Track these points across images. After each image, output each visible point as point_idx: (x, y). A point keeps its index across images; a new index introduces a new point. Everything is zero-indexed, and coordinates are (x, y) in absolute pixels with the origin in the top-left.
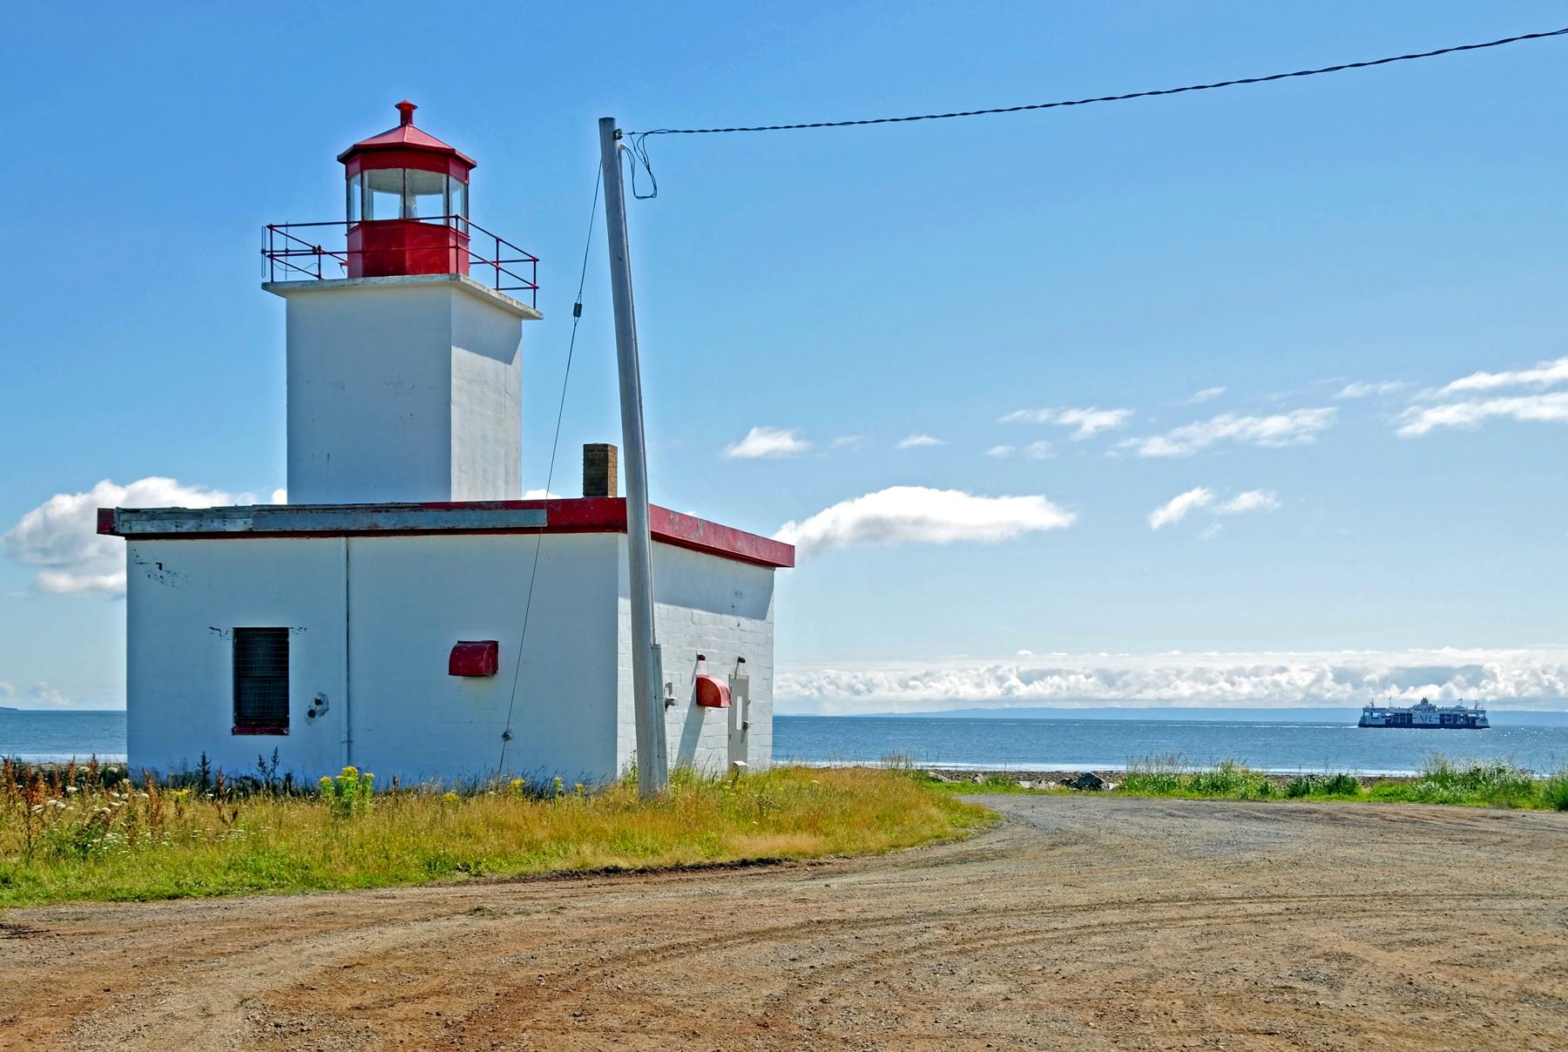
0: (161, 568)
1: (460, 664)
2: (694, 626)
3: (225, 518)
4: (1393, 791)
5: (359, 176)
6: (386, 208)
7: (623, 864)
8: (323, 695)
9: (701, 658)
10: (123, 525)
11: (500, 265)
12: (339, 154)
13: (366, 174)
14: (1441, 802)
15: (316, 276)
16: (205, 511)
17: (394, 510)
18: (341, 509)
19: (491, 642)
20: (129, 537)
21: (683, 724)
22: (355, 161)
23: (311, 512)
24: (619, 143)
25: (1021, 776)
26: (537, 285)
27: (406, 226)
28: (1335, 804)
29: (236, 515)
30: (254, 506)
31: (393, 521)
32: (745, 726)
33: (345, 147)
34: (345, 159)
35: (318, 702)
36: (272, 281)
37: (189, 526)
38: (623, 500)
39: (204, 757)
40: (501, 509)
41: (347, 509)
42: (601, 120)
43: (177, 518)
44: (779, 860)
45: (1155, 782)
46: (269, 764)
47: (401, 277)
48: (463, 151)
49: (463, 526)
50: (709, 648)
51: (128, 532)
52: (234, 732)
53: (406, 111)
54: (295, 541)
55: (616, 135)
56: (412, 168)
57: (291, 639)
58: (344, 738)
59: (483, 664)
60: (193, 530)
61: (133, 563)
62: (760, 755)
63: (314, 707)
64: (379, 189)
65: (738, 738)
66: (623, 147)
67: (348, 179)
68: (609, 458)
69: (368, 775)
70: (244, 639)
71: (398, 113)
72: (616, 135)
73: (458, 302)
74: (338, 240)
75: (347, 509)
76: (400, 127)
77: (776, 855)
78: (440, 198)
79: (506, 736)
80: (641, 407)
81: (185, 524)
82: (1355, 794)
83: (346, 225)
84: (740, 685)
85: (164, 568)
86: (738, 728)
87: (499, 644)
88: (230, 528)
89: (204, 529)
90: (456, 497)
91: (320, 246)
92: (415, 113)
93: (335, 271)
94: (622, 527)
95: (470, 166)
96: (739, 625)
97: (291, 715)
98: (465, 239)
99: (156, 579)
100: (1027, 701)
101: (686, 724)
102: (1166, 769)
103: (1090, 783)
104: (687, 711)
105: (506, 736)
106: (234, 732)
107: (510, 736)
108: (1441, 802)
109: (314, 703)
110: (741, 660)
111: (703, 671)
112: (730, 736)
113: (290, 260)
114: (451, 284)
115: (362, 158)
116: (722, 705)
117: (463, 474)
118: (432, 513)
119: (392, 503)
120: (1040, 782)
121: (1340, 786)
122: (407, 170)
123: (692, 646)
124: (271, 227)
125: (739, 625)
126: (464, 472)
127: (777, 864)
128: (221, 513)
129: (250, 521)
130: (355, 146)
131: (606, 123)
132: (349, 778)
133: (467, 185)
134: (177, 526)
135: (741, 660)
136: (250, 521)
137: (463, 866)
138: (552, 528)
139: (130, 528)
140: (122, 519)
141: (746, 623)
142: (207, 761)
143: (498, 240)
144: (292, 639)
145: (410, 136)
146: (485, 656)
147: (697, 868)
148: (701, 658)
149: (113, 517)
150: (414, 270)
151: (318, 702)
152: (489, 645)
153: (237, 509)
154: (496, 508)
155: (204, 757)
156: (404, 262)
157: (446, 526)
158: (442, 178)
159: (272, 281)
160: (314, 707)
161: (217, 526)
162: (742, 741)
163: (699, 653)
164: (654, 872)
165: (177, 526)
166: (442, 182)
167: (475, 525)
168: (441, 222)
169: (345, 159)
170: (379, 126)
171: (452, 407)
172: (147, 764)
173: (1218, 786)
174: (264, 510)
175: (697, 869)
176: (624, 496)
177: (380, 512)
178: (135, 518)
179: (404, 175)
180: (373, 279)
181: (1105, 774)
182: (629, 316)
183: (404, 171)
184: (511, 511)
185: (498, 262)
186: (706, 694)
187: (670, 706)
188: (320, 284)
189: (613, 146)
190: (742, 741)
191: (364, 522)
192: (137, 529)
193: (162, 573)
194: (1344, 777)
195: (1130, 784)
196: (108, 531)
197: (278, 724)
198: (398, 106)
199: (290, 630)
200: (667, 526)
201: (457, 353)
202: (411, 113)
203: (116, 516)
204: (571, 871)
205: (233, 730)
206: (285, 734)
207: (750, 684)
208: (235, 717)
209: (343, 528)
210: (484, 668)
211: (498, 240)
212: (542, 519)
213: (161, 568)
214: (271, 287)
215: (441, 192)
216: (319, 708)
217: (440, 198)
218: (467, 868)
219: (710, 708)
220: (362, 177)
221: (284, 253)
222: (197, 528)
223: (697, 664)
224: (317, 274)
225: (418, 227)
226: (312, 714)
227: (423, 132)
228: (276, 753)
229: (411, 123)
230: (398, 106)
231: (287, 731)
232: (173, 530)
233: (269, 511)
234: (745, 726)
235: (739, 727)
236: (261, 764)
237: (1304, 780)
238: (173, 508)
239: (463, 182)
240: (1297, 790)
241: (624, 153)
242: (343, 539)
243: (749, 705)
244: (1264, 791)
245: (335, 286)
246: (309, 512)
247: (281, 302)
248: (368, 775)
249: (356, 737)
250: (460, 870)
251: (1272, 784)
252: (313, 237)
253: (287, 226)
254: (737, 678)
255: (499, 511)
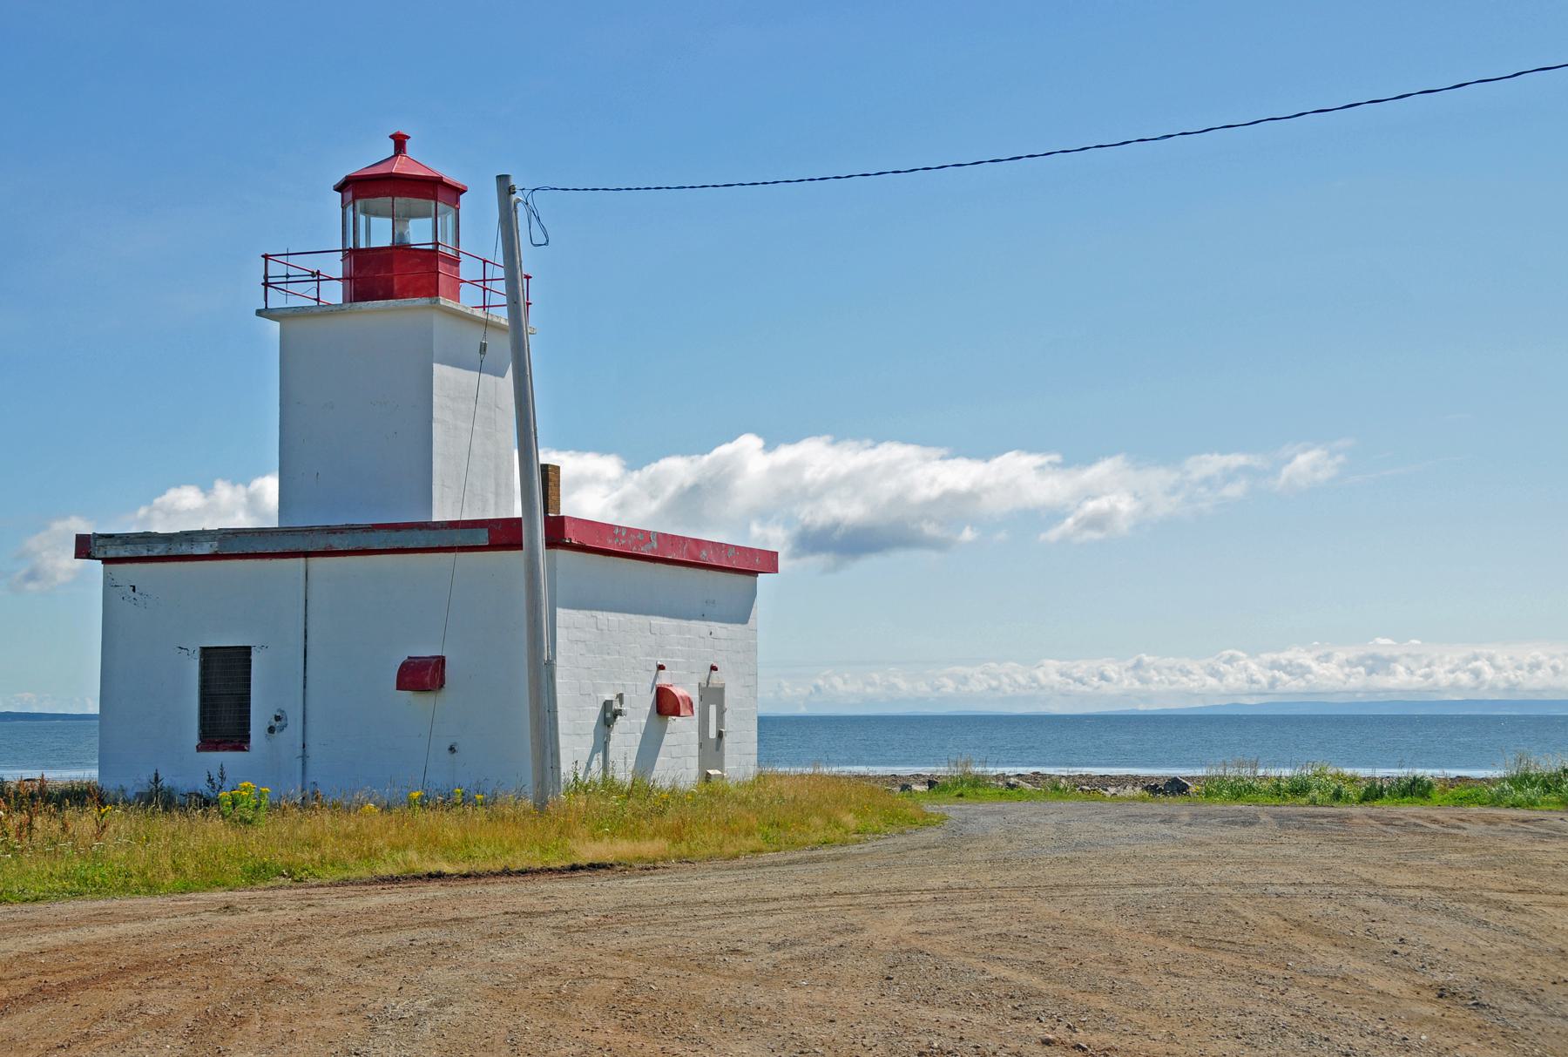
0: (134, 590)
1: (407, 679)
2: (653, 636)
3: (192, 541)
4: (1465, 792)
5: (352, 205)
6: (380, 234)
7: (447, 868)
8: (280, 710)
9: (661, 667)
10: (99, 550)
11: (488, 284)
12: (335, 184)
13: (359, 203)
14: (1512, 805)
15: (315, 299)
16: (174, 535)
17: (348, 531)
18: (298, 531)
19: (439, 657)
20: (106, 561)
21: (640, 736)
22: (348, 190)
23: (272, 535)
24: (514, 197)
25: (1105, 781)
26: (530, 301)
27: (400, 250)
28: (1409, 810)
29: (202, 538)
30: (220, 529)
31: (347, 542)
32: (720, 735)
33: (339, 178)
34: (340, 188)
35: (278, 718)
36: (266, 307)
37: (159, 550)
38: (519, 520)
39: (156, 774)
40: (446, 528)
41: (305, 531)
42: (498, 177)
43: (149, 543)
44: (611, 865)
45: (1231, 788)
46: (217, 780)
47: (385, 301)
48: (451, 175)
49: (411, 546)
50: (672, 658)
51: (103, 556)
52: (199, 749)
53: (400, 142)
54: (258, 562)
55: (511, 191)
56: (400, 196)
57: (253, 657)
58: (299, 752)
59: (428, 679)
60: (163, 554)
61: (109, 585)
62: (740, 762)
63: (274, 723)
64: (376, 215)
65: (713, 748)
66: (519, 200)
67: (344, 208)
68: (550, 477)
69: (264, 789)
70: (209, 656)
71: (392, 142)
72: (511, 191)
73: (439, 322)
74: (334, 266)
75: (305, 531)
76: (393, 157)
77: (610, 859)
78: (429, 221)
79: (452, 749)
80: (536, 438)
81: (157, 548)
82: (1429, 797)
83: (341, 253)
84: (713, 695)
85: (137, 590)
86: (711, 737)
87: (446, 659)
88: (197, 551)
89: (173, 553)
90: (438, 516)
91: (318, 271)
92: (408, 143)
93: (334, 293)
94: (518, 546)
95: (458, 191)
96: (711, 633)
97: (252, 732)
98: (455, 262)
99: (130, 601)
100: (1306, 694)
101: (644, 734)
102: (1246, 772)
103: (1177, 787)
104: (644, 721)
105: (452, 749)
106: (199, 749)
107: (456, 749)
108: (1512, 805)
109: (273, 720)
110: (713, 668)
111: (664, 680)
112: (701, 746)
113: (291, 287)
114: (433, 308)
115: (357, 188)
116: (682, 714)
117: (447, 489)
118: (383, 534)
119: (346, 525)
120: (1125, 788)
121: (1416, 789)
122: (397, 199)
123: (650, 656)
124: (266, 257)
125: (711, 633)
126: (448, 487)
127: (609, 869)
128: (188, 537)
129: (216, 544)
130: (347, 177)
131: (503, 179)
132: (244, 793)
133: (458, 209)
134: (148, 550)
135: (713, 668)
136: (216, 544)
137: (289, 873)
138: (493, 546)
139: (105, 553)
140: (97, 544)
141: (719, 628)
142: (159, 779)
143: (485, 262)
144: (254, 657)
145: (398, 167)
146: (430, 671)
147: (523, 873)
148: (661, 667)
149: (90, 542)
150: (403, 295)
151: (278, 718)
152: (435, 660)
153: (203, 533)
154: (442, 528)
155: (156, 774)
156: (393, 285)
157: (396, 546)
158: (431, 204)
159: (266, 307)
160: (274, 723)
161: (185, 549)
162: (717, 749)
163: (659, 663)
164: (478, 876)
165: (148, 550)
166: (431, 208)
167: (423, 545)
168: (430, 247)
169: (340, 188)
170: (371, 154)
171: (434, 425)
172: (111, 786)
173: (1299, 789)
174: (229, 533)
175: (523, 873)
176: (520, 516)
177: (335, 533)
178: (110, 543)
179: (393, 203)
180: (363, 305)
181: (1188, 778)
182: (524, 354)
183: (393, 200)
184: (455, 531)
185: (484, 280)
186: (666, 704)
187: (619, 718)
188: (322, 311)
189: (509, 201)
190: (717, 749)
191: (321, 543)
192: (112, 553)
193: (136, 595)
194: (1418, 780)
195: (1212, 788)
196: (84, 556)
197: (238, 739)
198: (392, 137)
199: (253, 648)
200: (610, 541)
201: (438, 369)
202: (404, 142)
203: (92, 541)
204: (392, 876)
205: (197, 747)
206: (245, 750)
207: (726, 694)
208: (200, 735)
209: (301, 550)
210: (429, 682)
211: (485, 262)
212: (483, 537)
213: (134, 590)
214: (265, 313)
215: (430, 216)
216: (278, 724)
217: (429, 221)
218: (291, 875)
219: (674, 717)
220: (354, 206)
221: (284, 279)
222: (167, 552)
223: (657, 674)
224: (316, 297)
225: (412, 252)
226: (271, 730)
227: (423, 159)
228: (222, 769)
229: (405, 153)
230: (392, 137)
231: (249, 747)
232: (145, 554)
233: (233, 534)
234: (720, 735)
235: (713, 734)
236: (210, 780)
237: (1379, 783)
238: (145, 533)
239: (454, 207)
240: (1373, 793)
241: (520, 206)
242: (302, 560)
243: (726, 714)
244: (1337, 795)
245: (330, 310)
246: (269, 535)
247: (275, 326)
248: (264, 789)
249: (311, 751)
250: (284, 876)
251: (1346, 789)
252: (312, 263)
253: (288, 254)
254: (710, 686)
255: (444, 531)
